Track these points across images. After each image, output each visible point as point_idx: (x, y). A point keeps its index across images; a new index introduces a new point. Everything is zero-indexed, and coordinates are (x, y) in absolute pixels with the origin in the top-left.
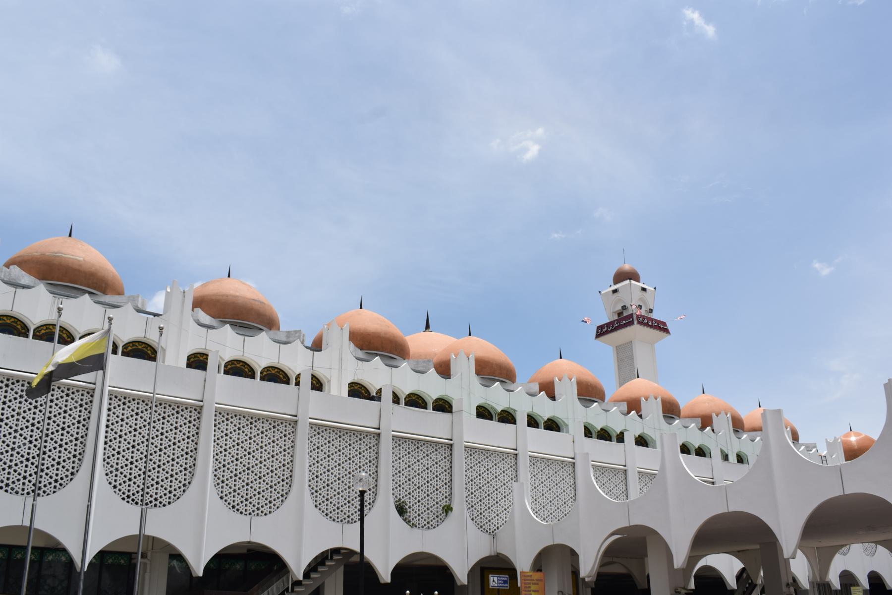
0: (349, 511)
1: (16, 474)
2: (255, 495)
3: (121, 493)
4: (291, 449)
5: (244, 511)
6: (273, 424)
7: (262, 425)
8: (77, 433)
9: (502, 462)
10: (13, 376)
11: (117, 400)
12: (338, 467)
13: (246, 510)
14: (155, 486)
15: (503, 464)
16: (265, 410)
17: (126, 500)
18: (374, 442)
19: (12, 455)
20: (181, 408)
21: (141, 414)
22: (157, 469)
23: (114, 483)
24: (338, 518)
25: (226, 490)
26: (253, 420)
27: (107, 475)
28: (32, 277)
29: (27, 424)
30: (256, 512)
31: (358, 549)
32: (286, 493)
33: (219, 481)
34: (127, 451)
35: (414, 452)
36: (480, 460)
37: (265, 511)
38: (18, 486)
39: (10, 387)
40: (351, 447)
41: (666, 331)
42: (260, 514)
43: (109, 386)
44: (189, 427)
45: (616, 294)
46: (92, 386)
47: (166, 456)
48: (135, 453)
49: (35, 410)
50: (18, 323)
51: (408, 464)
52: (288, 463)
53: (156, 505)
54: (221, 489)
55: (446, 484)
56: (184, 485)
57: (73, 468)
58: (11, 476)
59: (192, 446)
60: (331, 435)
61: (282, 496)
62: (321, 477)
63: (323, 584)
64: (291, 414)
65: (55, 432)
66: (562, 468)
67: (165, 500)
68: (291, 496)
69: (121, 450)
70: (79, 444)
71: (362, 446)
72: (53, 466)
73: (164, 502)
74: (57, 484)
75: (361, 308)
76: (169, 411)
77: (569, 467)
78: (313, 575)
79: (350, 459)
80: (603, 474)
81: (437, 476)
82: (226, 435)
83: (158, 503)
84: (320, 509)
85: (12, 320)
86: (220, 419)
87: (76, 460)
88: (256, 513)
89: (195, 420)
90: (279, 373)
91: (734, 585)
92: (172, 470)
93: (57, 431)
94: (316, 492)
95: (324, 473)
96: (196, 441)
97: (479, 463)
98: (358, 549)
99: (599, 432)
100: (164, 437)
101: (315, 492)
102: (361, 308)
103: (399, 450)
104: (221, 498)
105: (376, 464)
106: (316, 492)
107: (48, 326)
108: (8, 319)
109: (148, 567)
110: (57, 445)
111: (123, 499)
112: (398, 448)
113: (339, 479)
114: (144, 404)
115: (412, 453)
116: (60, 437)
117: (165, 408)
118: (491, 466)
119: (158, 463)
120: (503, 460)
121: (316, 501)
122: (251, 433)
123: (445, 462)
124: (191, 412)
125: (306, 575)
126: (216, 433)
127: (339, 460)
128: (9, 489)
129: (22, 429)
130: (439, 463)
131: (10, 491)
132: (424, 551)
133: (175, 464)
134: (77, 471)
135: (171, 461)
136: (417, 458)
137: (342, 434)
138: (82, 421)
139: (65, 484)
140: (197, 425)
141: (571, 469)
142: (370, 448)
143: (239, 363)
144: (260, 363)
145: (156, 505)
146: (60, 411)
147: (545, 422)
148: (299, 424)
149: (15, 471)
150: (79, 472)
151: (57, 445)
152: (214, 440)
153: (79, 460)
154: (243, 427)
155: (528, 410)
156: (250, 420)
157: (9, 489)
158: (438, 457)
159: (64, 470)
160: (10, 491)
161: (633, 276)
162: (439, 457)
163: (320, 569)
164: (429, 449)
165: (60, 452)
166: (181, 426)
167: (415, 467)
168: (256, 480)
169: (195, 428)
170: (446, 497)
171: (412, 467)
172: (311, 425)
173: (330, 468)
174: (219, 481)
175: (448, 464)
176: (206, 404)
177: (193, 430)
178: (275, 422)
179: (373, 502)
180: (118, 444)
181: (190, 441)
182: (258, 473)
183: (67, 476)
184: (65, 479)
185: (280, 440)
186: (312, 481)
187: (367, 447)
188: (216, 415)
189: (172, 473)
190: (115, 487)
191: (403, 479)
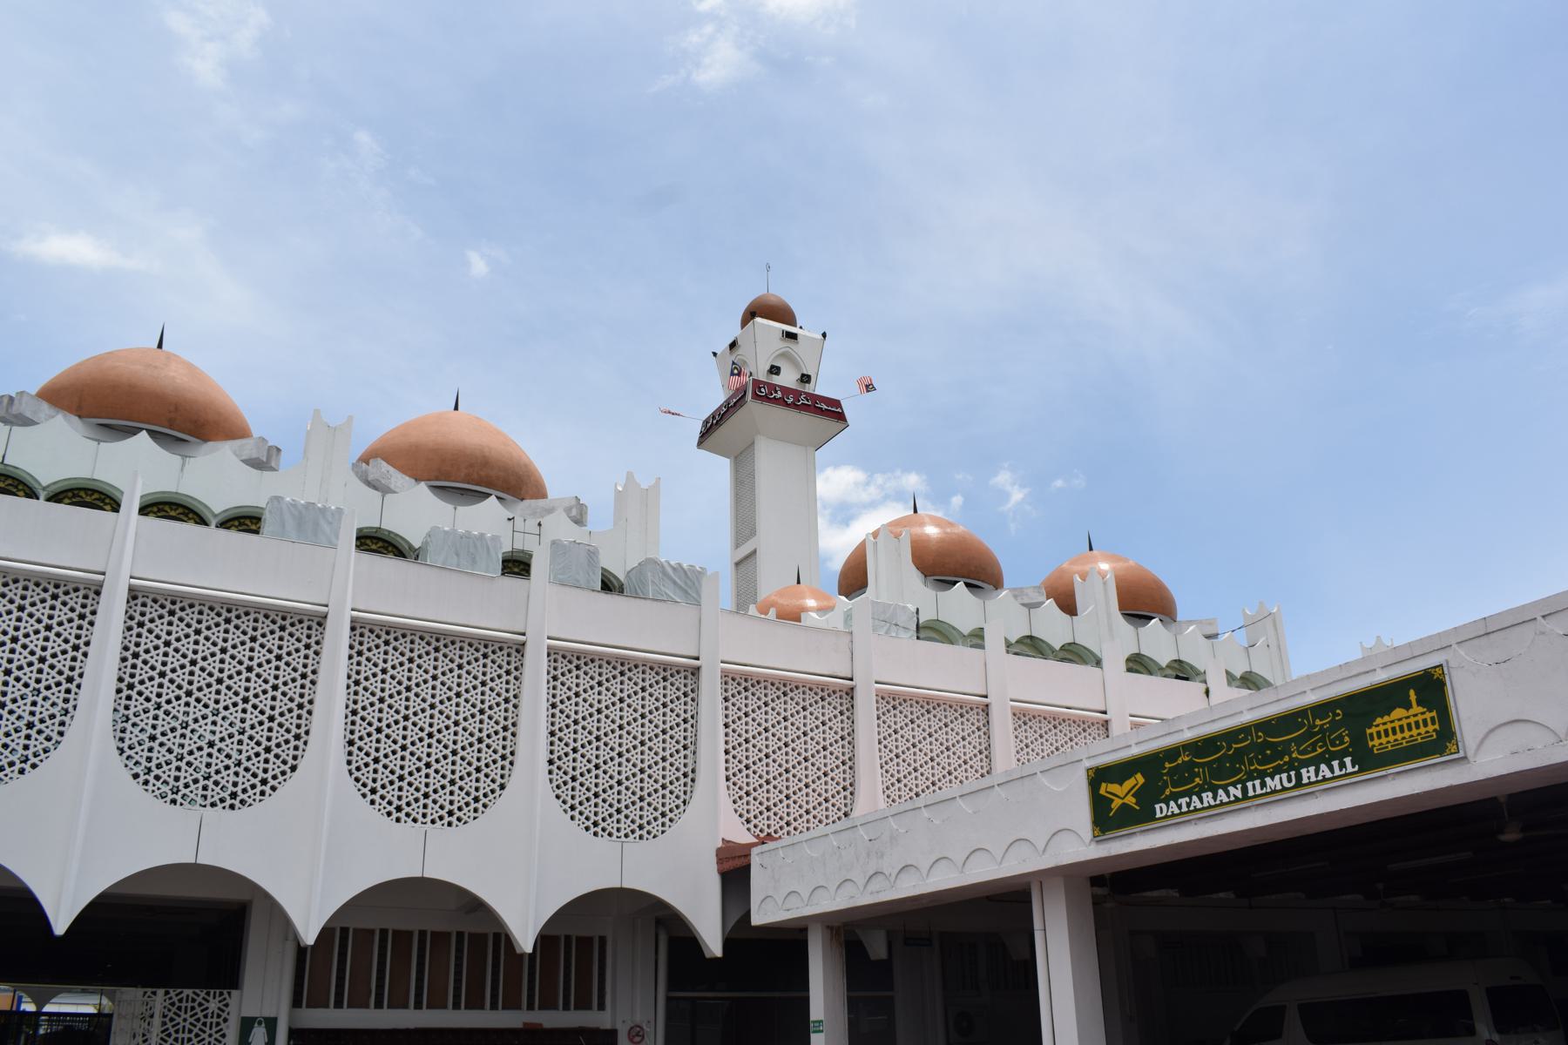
1: (278, 762)
9: (1083, 734)
10: (586, 653)
12: (822, 753)
15: (1056, 735)
21: (418, 661)
25: (485, 785)
26: (749, 684)
28: (407, 478)
30: (638, 833)
34: (494, 738)
35: (922, 719)
36: (1043, 732)
37: (654, 832)
39: (287, 631)
40: (915, 726)
41: (840, 417)
42: (646, 835)
43: (549, 638)
44: (599, 693)
45: (790, 343)
47: (416, 729)
48: (460, 735)
49: (278, 663)
50: (107, 501)
51: (912, 740)
53: (641, 837)
58: (379, 776)
60: (769, 692)
62: (754, 768)
64: (511, 629)
65: (303, 691)
66: (1025, 724)
69: (480, 794)
71: (898, 720)
76: (420, 647)
77: (978, 714)
80: (1055, 727)
81: (965, 763)
82: (665, 705)
83: (644, 832)
85: (10, 481)
86: (562, 666)
92: (574, 769)
95: (760, 760)
97: (1071, 740)
103: (823, 707)
107: (161, 507)
108: (171, 509)
112: (927, 716)
114: (653, 673)
115: (951, 726)
116: (367, 703)
117: (201, 613)
118: (937, 727)
120: (1084, 731)
123: (980, 737)
124: (201, 613)
126: (881, 730)
127: (824, 739)
128: (356, 659)
130: (1032, 746)
132: (625, 885)
133: (461, 732)
135: (476, 743)
136: (961, 734)
141: (980, 717)
143: (91, 495)
144: (218, 502)
146: (425, 676)
152: (879, 740)
156: (744, 684)
157: (356, 659)
158: (965, 727)
160: (36, 760)
161: (781, 313)
162: (969, 728)
164: (1042, 725)
171: (920, 746)
172: (725, 674)
173: (770, 750)
176: (530, 640)
178: (486, 647)
182: (638, 762)
188: (877, 702)
189: (574, 773)
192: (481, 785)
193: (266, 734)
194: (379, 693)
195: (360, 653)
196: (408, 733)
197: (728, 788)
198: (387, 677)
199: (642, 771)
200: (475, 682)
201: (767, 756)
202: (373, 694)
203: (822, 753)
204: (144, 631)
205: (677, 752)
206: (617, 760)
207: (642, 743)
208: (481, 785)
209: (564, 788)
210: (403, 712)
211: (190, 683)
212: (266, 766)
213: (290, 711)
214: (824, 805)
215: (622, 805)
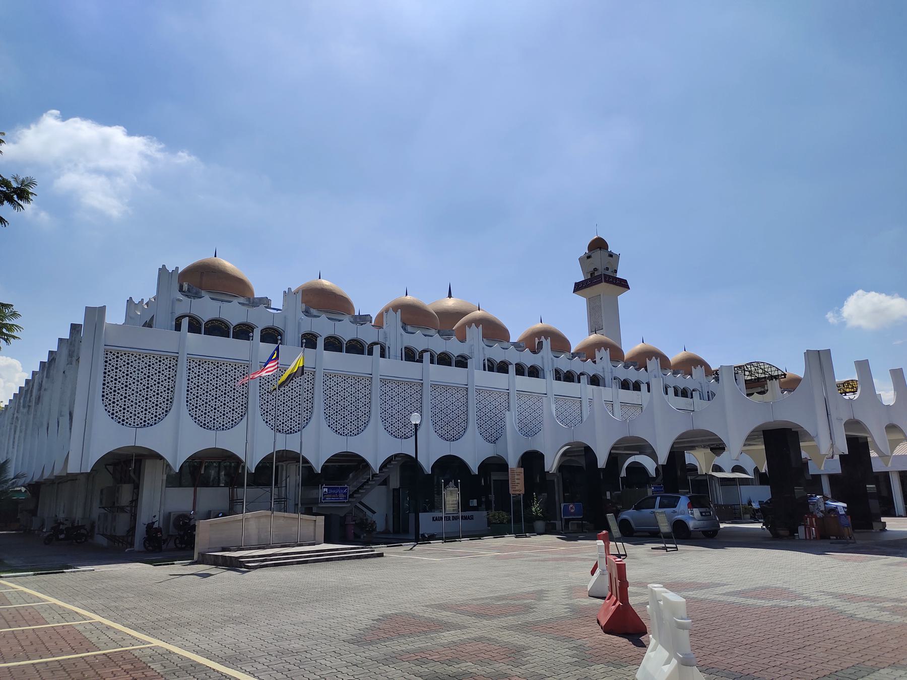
0: (405, 431)
2: (348, 424)
3: (270, 426)
4: (369, 395)
5: (342, 433)
6: (344, 378)
7: (351, 381)
8: (243, 391)
11: (112, 354)
13: (344, 433)
14: (290, 421)
16: (158, 350)
17: (122, 423)
18: (419, 388)
19: (206, 407)
20: (142, 356)
22: (290, 411)
23: (266, 420)
24: (398, 435)
27: (262, 415)
29: (213, 387)
31: (414, 456)
32: (367, 422)
33: (327, 416)
38: (131, 421)
41: (629, 288)
46: (177, 355)
52: (368, 403)
54: (328, 421)
55: (464, 413)
56: (241, 416)
57: (167, 407)
59: (310, 396)
61: (365, 423)
63: (389, 476)
67: (152, 421)
68: (370, 424)
69: (269, 400)
70: (170, 392)
72: (230, 411)
73: (296, 430)
74: (157, 419)
75: (320, 278)
78: (384, 470)
79: (405, 399)
84: (387, 430)
87: (169, 402)
88: (349, 434)
89: (311, 380)
90: (275, 332)
91: (476, 469)
93: (231, 391)
94: (385, 420)
96: (312, 392)
98: (414, 456)
99: (565, 373)
100: (293, 391)
101: (384, 420)
102: (320, 278)
104: (329, 426)
105: (421, 402)
106: (385, 420)
109: (285, 467)
110: (157, 392)
111: (201, 426)
113: (398, 412)
117: (209, 364)
119: (291, 407)
121: (385, 426)
122: (344, 386)
125: (381, 469)
128: (125, 423)
129: (210, 391)
131: (125, 424)
133: (235, 402)
134: (170, 409)
137: (399, 384)
138: (129, 374)
139: (237, 422)
140: (313, 383)
142: (417, 392)
145: (223, 429)
147: (326, 339)
148: (424, 385)
149: (208, 416)
150: (171, 410)
151: (231, 399)
153: (171, 402)
154: (340, 383)
155: (330, 332)
157: (125, 423)
159: (237, 414)
160: (125, 424)
163: (388, 466)
165: (267, 405)
166: (333, 386)
167: (445, 403)
168: (349, 414)
169: (311, 385)
170: (464, 421)
174: (327, 416)
175: (507, 404)
177: (310, 386)
179: (310, 418)
180: (233, 394)
181: (309, 392)
183: (163, 413)
184: (238, 419)
185: (362, 389)
186: (382, 414)
187: (403, 390)
190: (267, 422)
191: (437, 411)
192: (217, 403)
193: (201, 404)
194: (214, 406)
195: (123, 420)
196: (235, 405)
197: (187, 405)
198: (198, 399)
199: (284, 403)
200: (237, 400)
201: (392, 389)
202: (228, 406)
203: (410, 389)
204: (158, 407)
205: (342, 391)
206: (290, 421)
207: (365, 387)
208: (217, 403)
209: (272, 401)
210: (145, 408)
211: (156, 409)
212: (119, 411)
213: (203, 405)
214: (385, 395)
215: (269, 400)
